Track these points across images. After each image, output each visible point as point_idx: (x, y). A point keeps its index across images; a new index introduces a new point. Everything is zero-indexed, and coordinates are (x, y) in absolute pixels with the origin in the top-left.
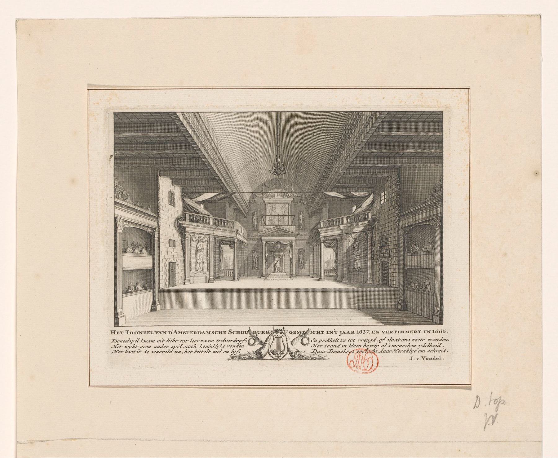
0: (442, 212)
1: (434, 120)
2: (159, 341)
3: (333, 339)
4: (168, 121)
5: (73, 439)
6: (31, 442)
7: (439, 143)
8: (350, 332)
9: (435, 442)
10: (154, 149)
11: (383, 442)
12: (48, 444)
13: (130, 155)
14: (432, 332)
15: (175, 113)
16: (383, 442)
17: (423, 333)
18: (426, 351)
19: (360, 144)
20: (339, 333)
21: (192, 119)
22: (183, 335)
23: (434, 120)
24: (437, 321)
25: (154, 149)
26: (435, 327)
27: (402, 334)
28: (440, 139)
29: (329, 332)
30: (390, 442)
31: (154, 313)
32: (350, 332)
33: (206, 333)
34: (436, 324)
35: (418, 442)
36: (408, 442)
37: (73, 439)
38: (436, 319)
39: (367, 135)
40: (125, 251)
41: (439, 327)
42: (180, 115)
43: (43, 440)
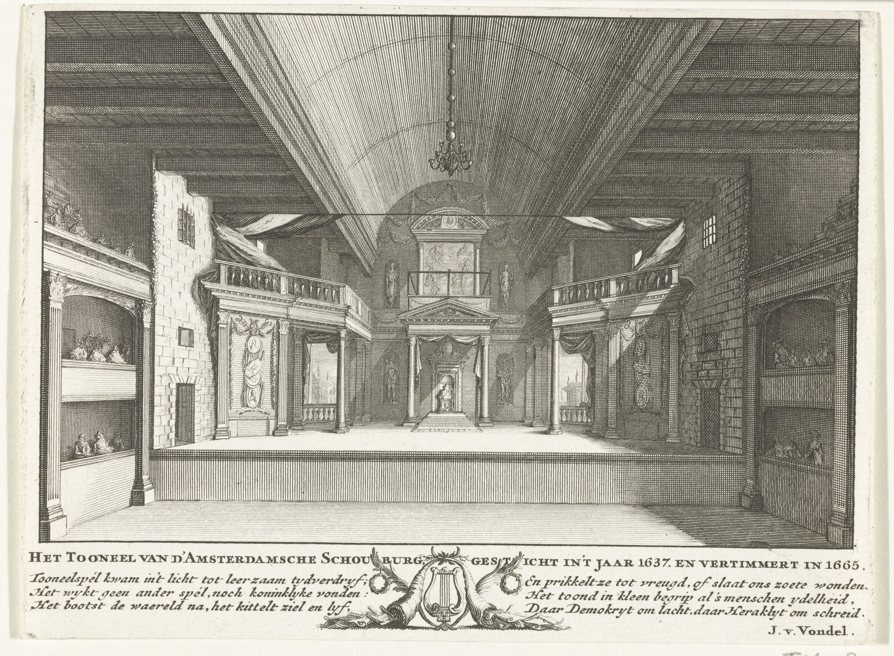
4: (182, 34)
8: (623, 563)
14: (824, 565)
29: (570, 563)
32: (623, 563)
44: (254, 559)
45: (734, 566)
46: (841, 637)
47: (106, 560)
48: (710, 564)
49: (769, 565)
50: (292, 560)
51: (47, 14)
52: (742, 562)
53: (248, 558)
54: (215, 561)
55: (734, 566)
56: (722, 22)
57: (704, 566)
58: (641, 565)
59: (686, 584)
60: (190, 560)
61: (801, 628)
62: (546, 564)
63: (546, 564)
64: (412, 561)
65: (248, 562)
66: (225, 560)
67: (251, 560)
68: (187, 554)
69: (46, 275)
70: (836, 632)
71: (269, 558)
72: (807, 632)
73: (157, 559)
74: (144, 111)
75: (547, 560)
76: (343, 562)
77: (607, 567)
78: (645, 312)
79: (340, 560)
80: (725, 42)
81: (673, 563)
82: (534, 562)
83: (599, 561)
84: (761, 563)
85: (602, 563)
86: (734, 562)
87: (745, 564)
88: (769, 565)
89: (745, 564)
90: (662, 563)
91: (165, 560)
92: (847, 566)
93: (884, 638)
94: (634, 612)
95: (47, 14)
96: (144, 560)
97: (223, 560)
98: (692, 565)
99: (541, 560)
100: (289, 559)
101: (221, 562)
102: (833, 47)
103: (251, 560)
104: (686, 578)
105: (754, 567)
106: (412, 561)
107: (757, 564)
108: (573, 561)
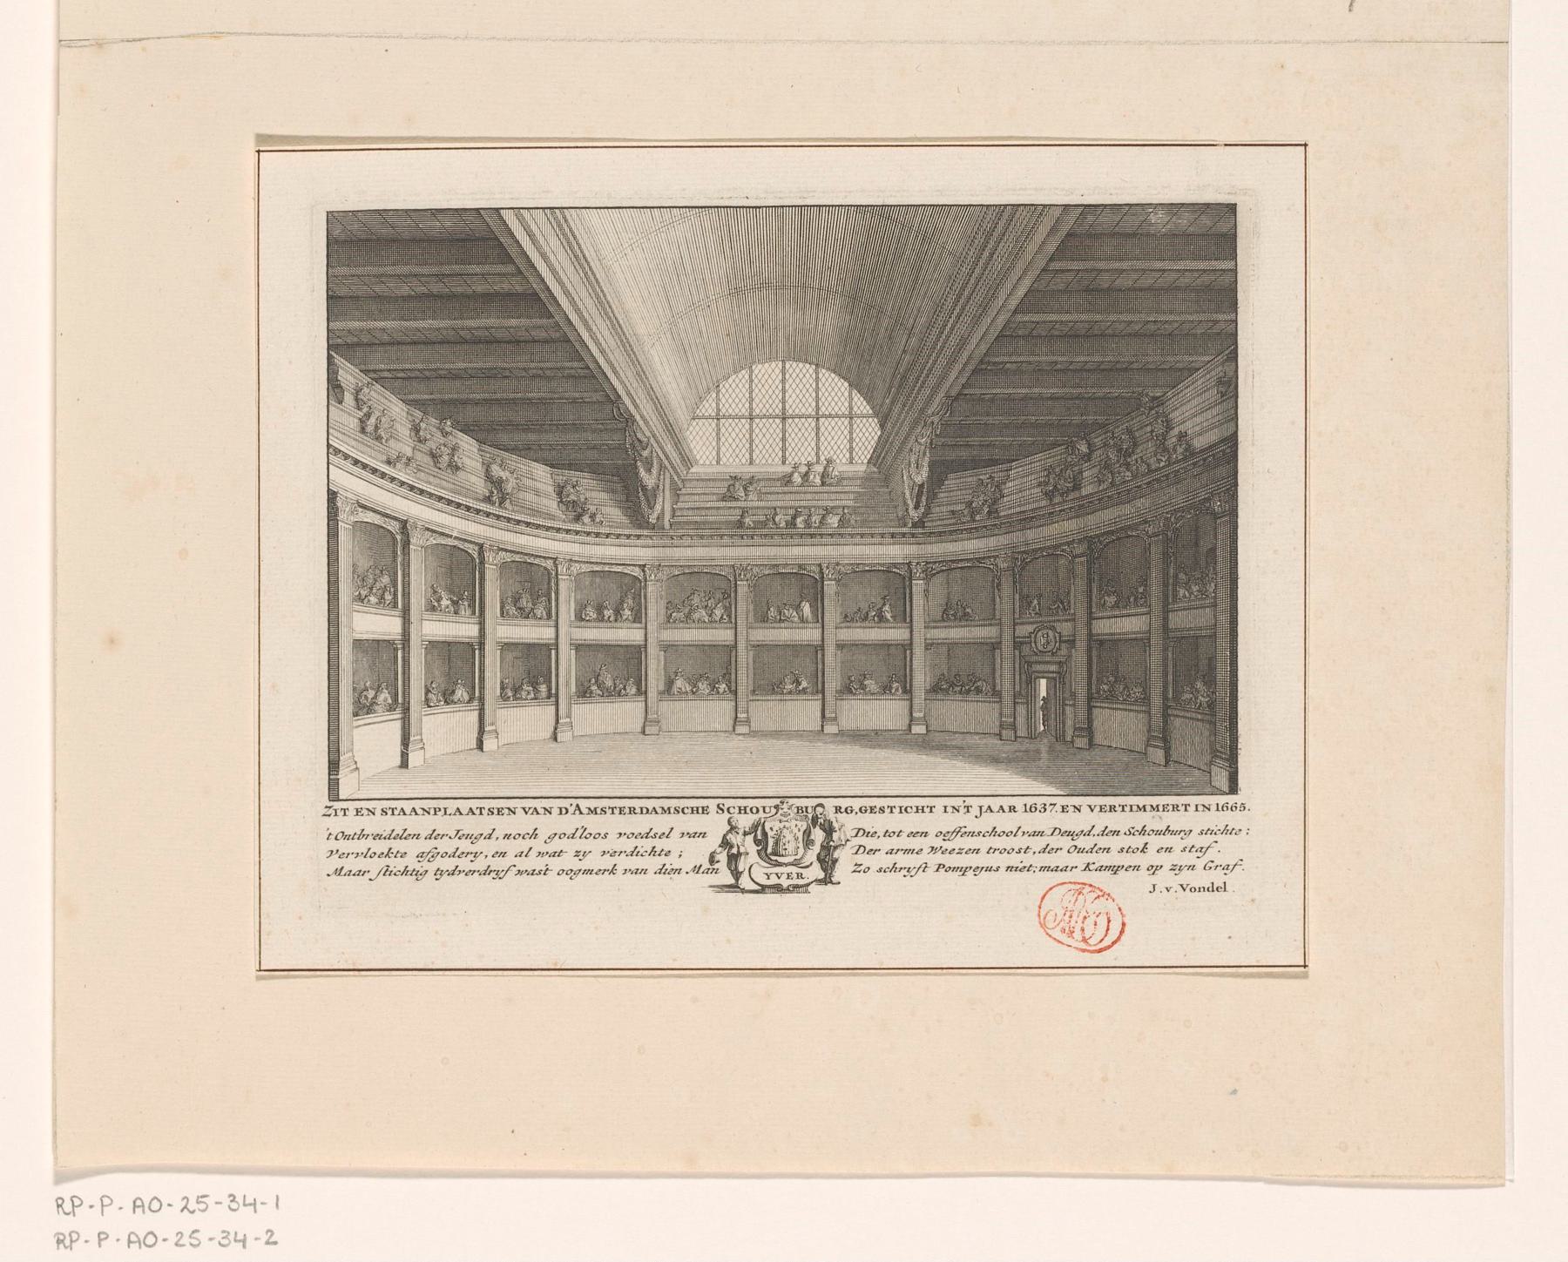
0: (1235, 435)
1: (1212, 232)
5: (216, 35)
6: (100, 44)
7: (1226, 296)
9: (1214, 42)
10: (448, 316)
11: (1070, 43)
12: (144, 49)
14: (1214, 808)
16: (1070, 43)
17: (1192, 815)
21: (539, 223)
23: (1212, 232)
25: (448, 316)
28: (1227, 278)
30: (1089, 43)
34: (1217, 792)
35: (1168, 43)
36: (1140, 43)
37: (216, 35)
38: (1221, 779)
39: (1025, 272)
40: (427, 702)
41: (1231, 799)
42: (509, 217)
43: (130, 37)
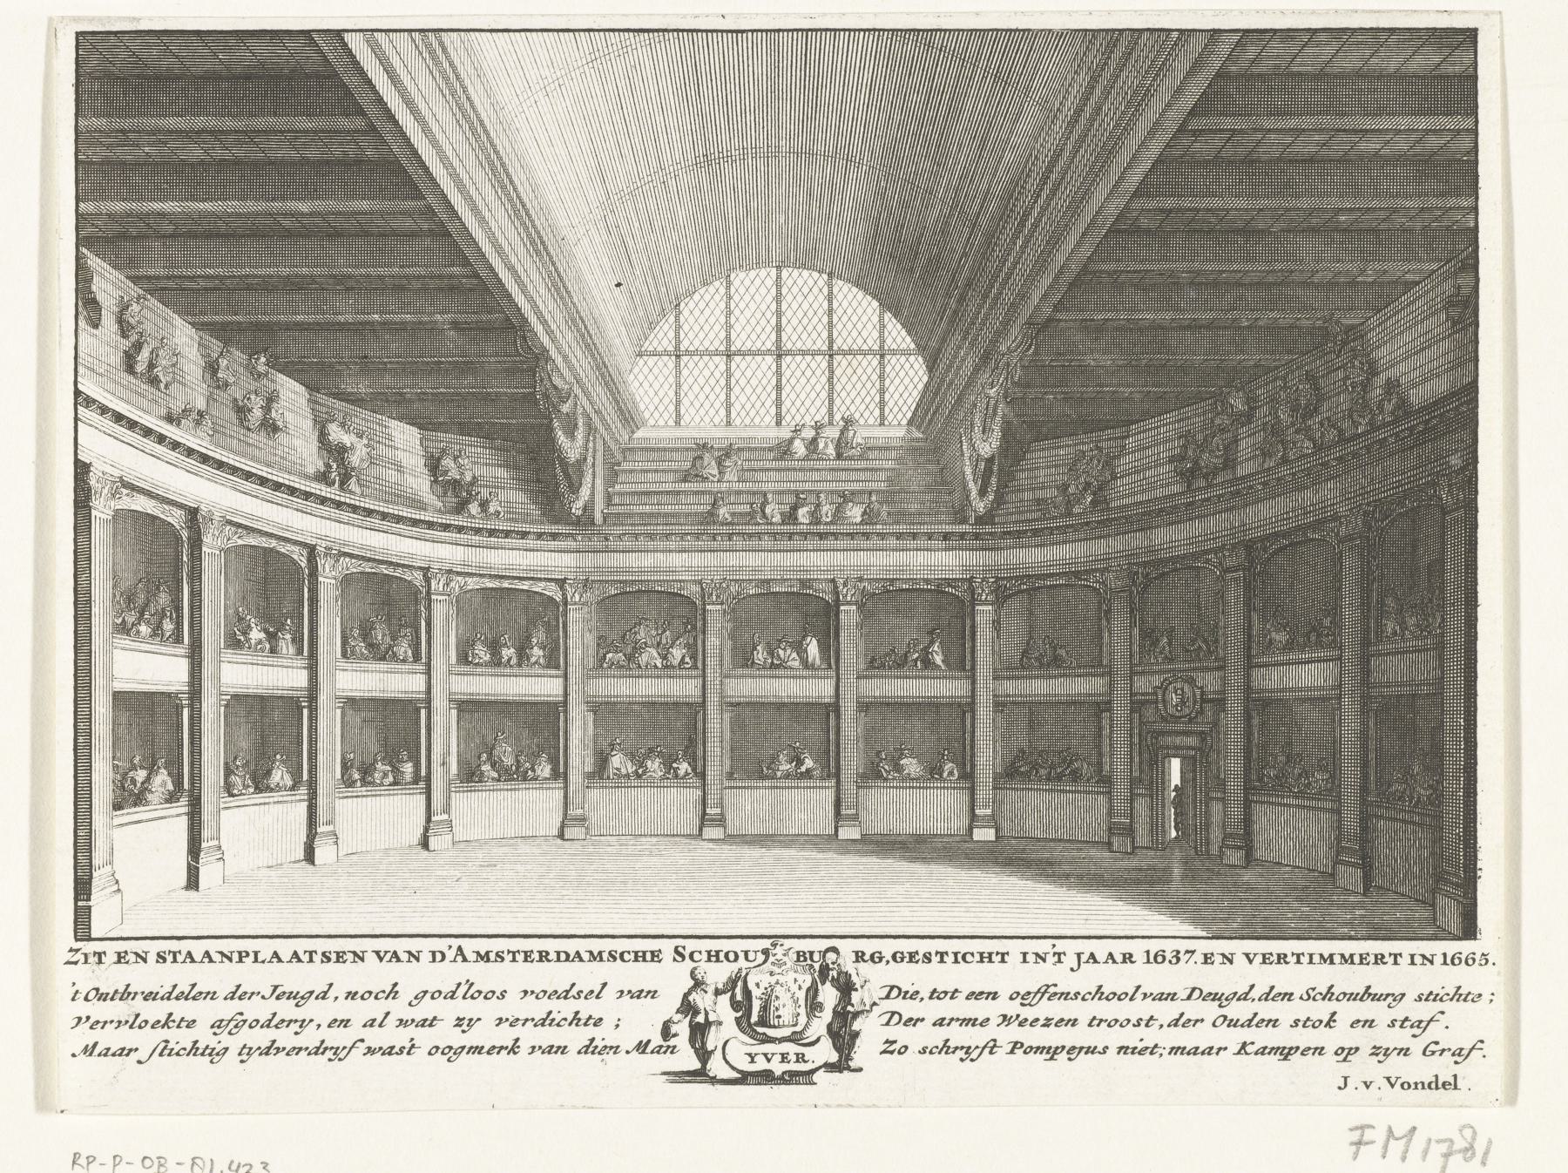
2: (1309, 996)
3: (1336, 991)
4: (306, 76)
8: (1119, 958)
13: (286, 223)
14: (1439, 960)
15: (338, 34)
17: (1410, 969)
18: (1084, 1021)
19: (1152, 133)
20: (1070, 960)
22: (606, 965)
24: (1455, 925)
26: (1451, 947)
27: (1326, 966)
29: (1418, 960)
31: (192, 893)
32: (1119, 958)
33: (586, 956)
38: (1450, 915)
41: (1465, 947)
44: (568, 955)
45: (1298, 962)
46: (1451, 1093)
47: (230, 959)
48: (1259, 959)
49: (1357, 959)
50: (626, 956)
51: (1476, 30)
52: (1311, 956)
53: (558, 953)
54: (165, 960)
55: (1298, 962)
56: (1236, 37)
57: (1251, 961)
58: (1445, 963)
59: (331, 994)
60: (459, 958)
61: (1388, 1079)
62: (990, 961)
63: (990, 961)
64: (867, 957)
65: (558, 960)
66: (520, 957)
67: (563, 957)
68: (184, 953)
69: (82, 470)
70: (1444, 1084)
71: (591, 953)
72: (1398, 1086)
73: (217, 957)
74: (258, 201)
75: (990, 954)
76: (636, 960)
77: (1091, 966)
78: (252, 517)
79: (632, 956)
80: (1247, 73)
81: (1199, 957)
82: (969, 958)
83: (1079, 955)
84: (1343, 956)
85: (1084, 958)
86: (1298, 956)
87: (1316, 959)
88: (1357, 959)
89: (1316, 959)
90: (1184, 958)
91: (417, 959)
92: (1469, 961)
93: (1512, 1097)
94: (420, 1054)
95: (1476, 30)
96: (381, 959)
97: (315, 957)
98: (362, 959)
99: (981, 954)
100: (622, 955)
101: (514, 960)
102: (1443, 72)
103: (563, 957)
104: (331, 985)
105: (1332, 962)
106: (867, 957)
107: (1337, 959)
108: (1424, 957)
